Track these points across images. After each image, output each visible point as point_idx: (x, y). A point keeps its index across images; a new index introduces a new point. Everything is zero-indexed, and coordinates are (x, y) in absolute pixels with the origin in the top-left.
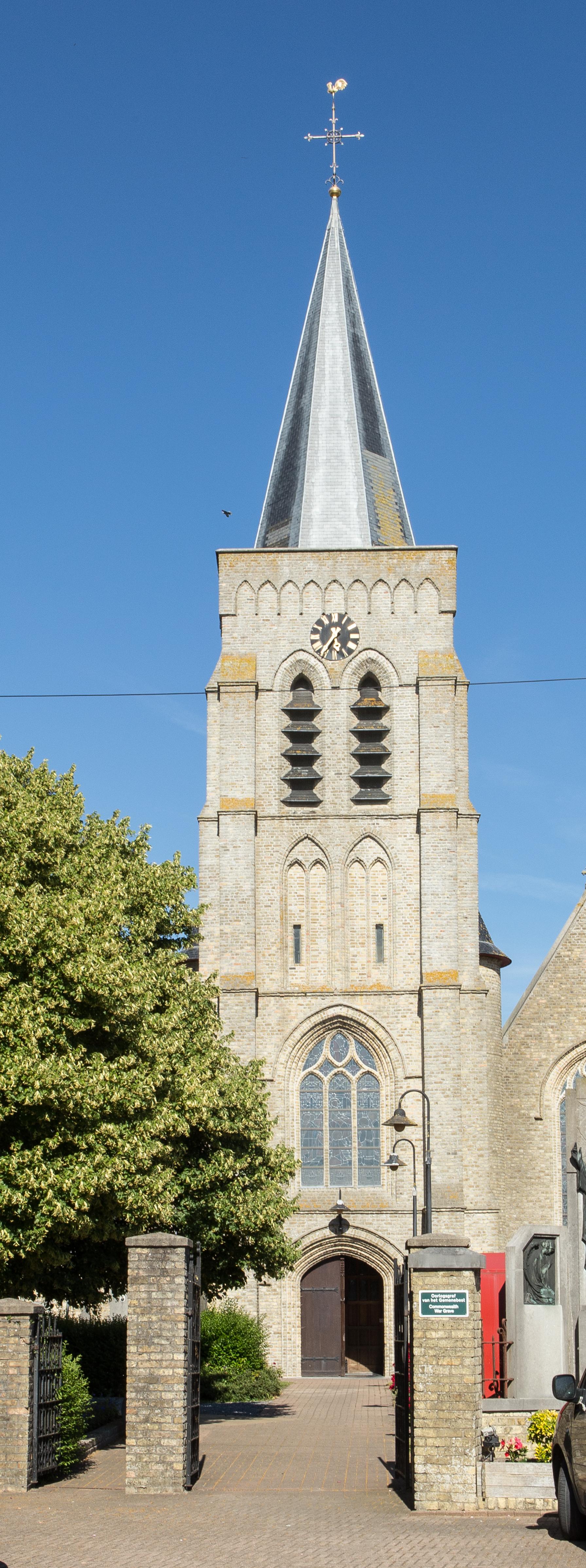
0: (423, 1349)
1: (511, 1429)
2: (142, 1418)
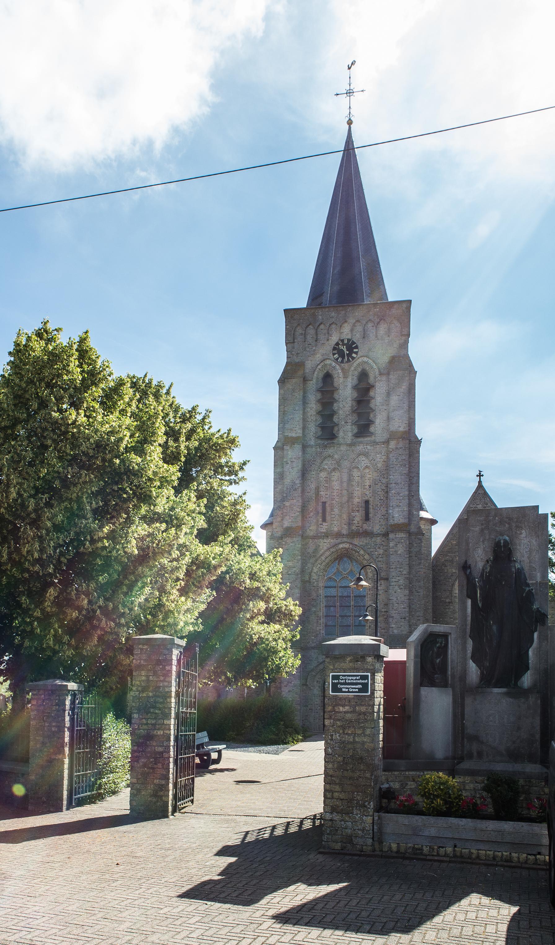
0: (332, 721)
1: (407, 784)
2: (141, 764)
